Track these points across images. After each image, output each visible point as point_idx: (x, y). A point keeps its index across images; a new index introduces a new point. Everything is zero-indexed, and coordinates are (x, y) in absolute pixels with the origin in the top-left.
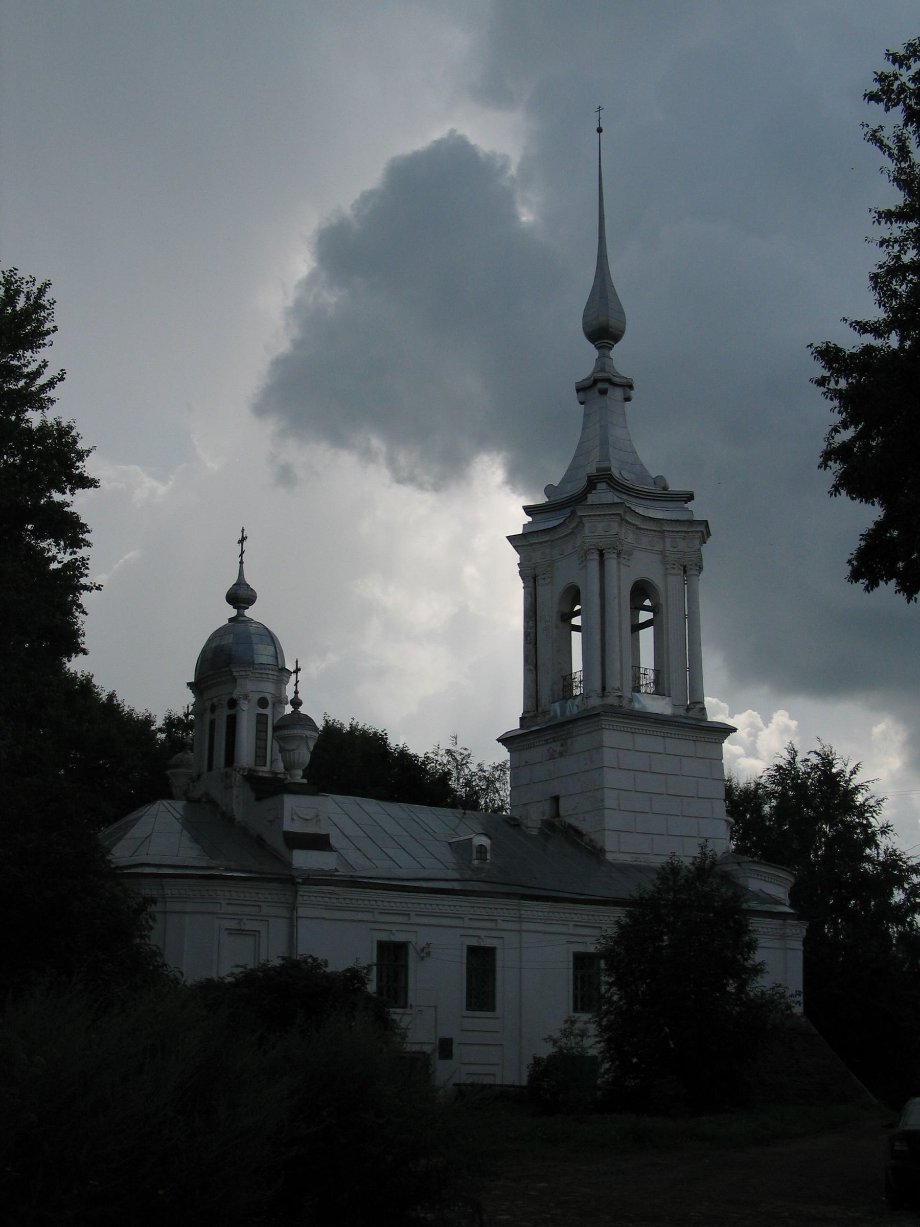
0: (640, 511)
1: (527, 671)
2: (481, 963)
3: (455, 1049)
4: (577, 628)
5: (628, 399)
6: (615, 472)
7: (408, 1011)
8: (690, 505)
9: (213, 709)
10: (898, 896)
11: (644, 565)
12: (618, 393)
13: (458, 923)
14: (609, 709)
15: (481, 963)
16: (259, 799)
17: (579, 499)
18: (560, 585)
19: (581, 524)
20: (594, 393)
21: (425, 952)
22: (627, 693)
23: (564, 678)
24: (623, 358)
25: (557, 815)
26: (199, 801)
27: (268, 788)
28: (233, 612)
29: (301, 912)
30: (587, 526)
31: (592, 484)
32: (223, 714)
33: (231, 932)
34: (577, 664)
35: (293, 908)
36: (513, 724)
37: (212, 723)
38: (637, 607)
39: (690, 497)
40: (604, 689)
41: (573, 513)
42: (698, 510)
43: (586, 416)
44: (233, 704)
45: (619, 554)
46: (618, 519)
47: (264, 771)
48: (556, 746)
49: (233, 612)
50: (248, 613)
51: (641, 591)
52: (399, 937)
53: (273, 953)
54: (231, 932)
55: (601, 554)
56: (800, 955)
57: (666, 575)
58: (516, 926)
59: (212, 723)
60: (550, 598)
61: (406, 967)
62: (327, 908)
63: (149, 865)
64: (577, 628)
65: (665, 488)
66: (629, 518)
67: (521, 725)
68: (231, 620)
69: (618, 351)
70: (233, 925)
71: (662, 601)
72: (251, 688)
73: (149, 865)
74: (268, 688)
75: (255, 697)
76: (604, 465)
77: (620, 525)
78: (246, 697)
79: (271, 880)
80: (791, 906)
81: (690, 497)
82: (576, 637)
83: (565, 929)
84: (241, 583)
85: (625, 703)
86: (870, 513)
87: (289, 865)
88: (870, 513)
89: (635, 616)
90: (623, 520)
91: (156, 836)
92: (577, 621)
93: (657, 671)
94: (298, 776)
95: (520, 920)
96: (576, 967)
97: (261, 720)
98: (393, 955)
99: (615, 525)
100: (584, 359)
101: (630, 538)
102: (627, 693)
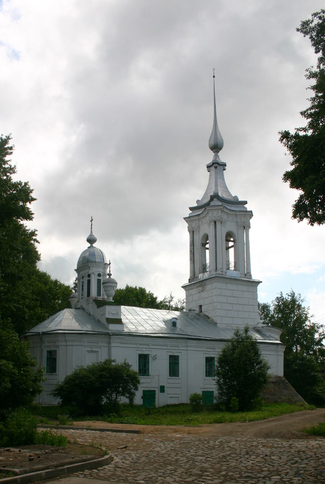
0: (229, 208)
1: (191, 263)
2: (174, 361)
3: (165, 389)
4: (207, 249)
5: (224, 170)
6: (220, 194)
7: (149, 377)
8: (246, 206)
9: (83, 278)
10: (317, 336)
11: (231, 226)
12: (222, 168)
13: (166, 348)
14: (221, 277)
15: (174, 361)
16: (98, 307)
17: (208, 204)
18: (202, 234)
19: (208, 212)
20: (213, 168)
21: (155, 358)
22: (225, 270)
23: (203, 265)
24: (223, 157)
25: (201, 312)
26: (79, 308)
27: (101, 304)
28: (89, 245)
29: (112, 345)
30: (210, 213)
31: (212, 198)
32: (86, 279)
33: (88, 352)
34: (208, 261)
35: (109, 343)
36: (186, 282)
37: (83, 282)
38: (228, 241)
39: (246, 203)
40: (216, 269)
41: (205, 209)
42: (248, 207)
43: (210, 176)
44: (89, 276)
45: (221, 223)
46: (220, 210)
47: (100, 298)
48: (201, 288)
49: (89, 245)
50: (94, 245)
51: (229, 236)
52: (146, 353)
53: (102, 358)
54: (88, 352)
55: (215, 222)
56: (283, 357)
57: (238, 229)
58: (65, 344)
59: (83, 282)
60: (198, 243)
61: (148, 362)
62: (121, 343)
63: (61, 330)
64: (207, 249)
65: (237, 199)
66: (224, 210)
67: (189, 282)
68: (89, 248)
69: (220, 154)
70: (89, 349)
71: (236, 239)
72: (94, 270)
73: (61, 330)
74: (101, 271)
75: (97, 274)
76: (216, 192)
77: (222, 213)
78: (93, 273)
79: (101, 334)
80: (281, 341)
81: (246, 203)
82: (207, 251)
83: (166, 348)
84: (91, 235)
85: (224, 273)
86: (298, 193)
87: (108, 329)
88: (298, 193)
89: (227, 244)
90: (222, 211)
91: (66, 320)
92: (207, 246)
93: (235, 263)
94: (111, 299)
95: (187, 346)
96: (206, 362)
97: (99, 281)
98: (144, 359)
99: (220, 212)
100: (210, 157)
101: (225, 217)
102: (225, 270)
